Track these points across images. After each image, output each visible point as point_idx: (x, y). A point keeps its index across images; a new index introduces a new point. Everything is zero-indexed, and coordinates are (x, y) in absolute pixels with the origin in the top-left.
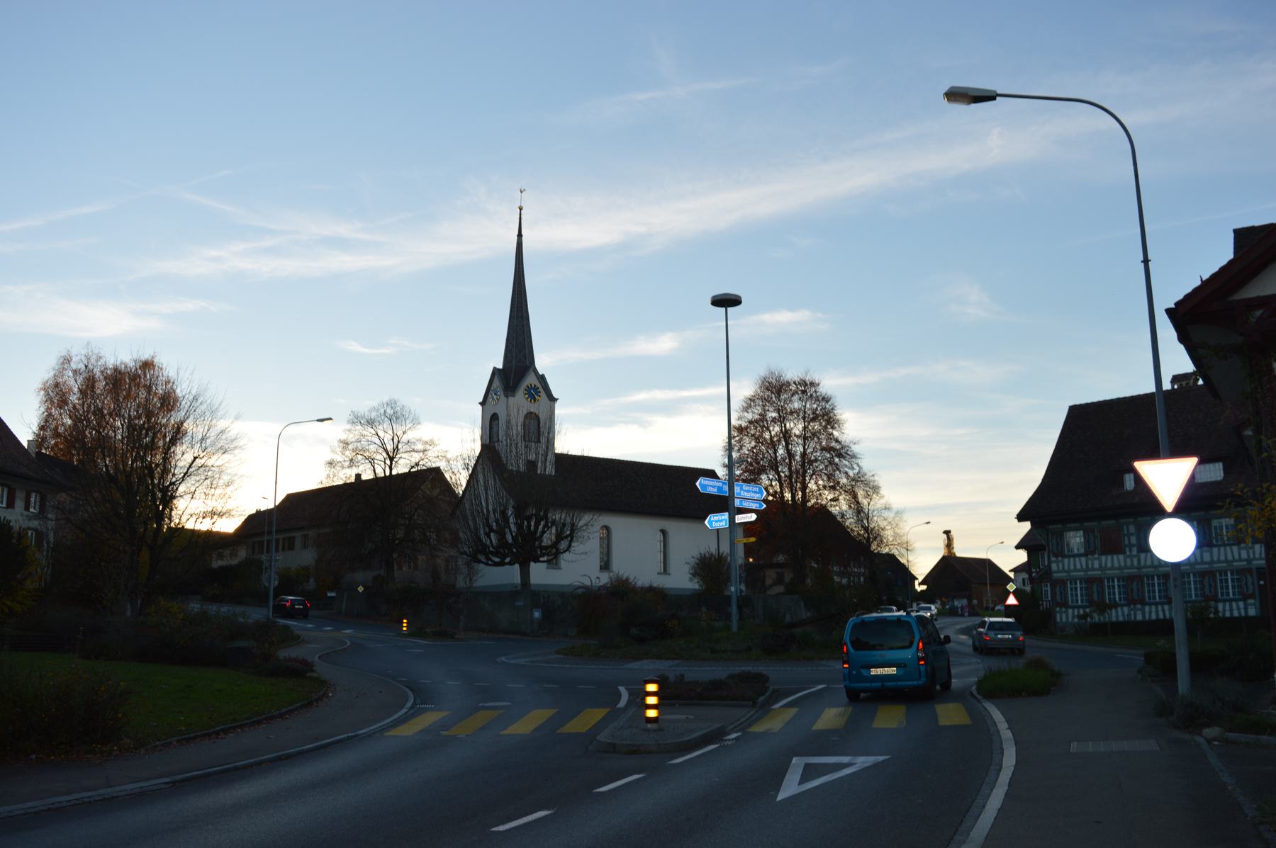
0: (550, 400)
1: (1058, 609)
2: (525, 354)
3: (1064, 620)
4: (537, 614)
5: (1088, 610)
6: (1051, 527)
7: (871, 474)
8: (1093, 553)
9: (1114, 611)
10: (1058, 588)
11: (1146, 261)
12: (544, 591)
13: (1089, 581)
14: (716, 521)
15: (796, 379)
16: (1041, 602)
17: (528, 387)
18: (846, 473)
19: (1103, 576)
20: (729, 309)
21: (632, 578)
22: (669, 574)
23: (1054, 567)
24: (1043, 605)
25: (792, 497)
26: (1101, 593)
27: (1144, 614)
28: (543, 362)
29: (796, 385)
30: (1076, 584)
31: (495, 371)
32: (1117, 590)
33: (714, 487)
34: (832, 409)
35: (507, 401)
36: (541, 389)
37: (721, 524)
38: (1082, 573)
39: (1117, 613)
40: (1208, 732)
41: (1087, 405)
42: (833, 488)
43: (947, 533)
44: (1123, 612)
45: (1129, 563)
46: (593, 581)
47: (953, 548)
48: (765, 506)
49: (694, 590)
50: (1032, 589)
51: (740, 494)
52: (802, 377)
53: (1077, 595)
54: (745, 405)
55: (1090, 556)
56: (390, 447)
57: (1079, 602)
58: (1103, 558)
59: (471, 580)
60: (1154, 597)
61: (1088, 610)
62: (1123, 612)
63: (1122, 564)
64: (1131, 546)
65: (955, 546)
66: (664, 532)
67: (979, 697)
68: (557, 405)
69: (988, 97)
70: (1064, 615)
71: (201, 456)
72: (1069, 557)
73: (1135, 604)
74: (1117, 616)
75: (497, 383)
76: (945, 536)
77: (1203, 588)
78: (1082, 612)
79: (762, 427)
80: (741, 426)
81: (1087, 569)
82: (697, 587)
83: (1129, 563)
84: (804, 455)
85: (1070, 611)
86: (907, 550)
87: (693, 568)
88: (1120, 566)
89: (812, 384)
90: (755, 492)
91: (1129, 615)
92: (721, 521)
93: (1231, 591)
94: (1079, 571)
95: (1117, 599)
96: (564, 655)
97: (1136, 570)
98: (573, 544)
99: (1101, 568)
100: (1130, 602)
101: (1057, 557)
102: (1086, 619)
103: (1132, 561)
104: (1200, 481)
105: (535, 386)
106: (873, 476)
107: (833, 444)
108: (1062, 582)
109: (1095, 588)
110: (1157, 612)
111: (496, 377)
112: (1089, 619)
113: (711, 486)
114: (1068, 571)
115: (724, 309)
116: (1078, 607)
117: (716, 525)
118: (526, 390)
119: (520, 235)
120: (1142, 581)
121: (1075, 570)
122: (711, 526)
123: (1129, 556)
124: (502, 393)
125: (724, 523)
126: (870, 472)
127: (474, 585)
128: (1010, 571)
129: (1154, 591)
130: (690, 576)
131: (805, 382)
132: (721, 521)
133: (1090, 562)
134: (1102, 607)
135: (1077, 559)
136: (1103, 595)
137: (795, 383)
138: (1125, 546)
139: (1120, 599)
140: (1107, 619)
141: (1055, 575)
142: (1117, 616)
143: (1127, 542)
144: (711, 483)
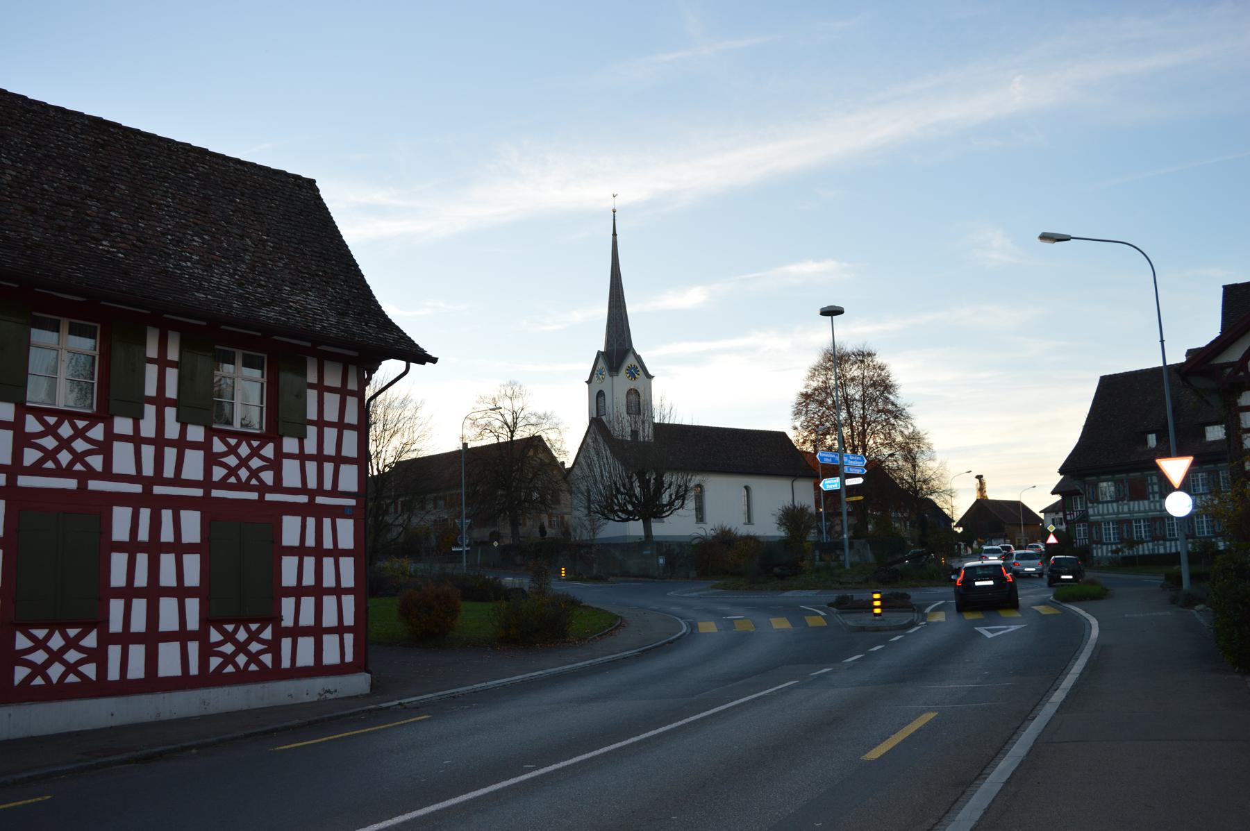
0: (647, 378)
1: (1094, 546)
3: (1100, 554)
4: (661, 561)
5: (1119, 546)
6: (1087, 479)
7: (924, 433)
8: (1123, 500)
9: (1141, 546)
10: (1094, 529)
11: (1162, 341)
12: (666, 542)
13: (1120, 523)
14: (830, 484)
15: (855, 350)
16: (1075, 541)
18: (902, 432)
19: (1131, 518)
20: (834, 317)
21: (733, 529)
22: (753, 524)
23: (1091, 511)
24: (1076, 542)
26: (1130, 532)
27: (1165, 548)
28: (640, 343)
29: (855, 355)
30: (1109, 525)
31: (599, 354)
32: (1143, 529)
33: (829, 458)
34: (888, 376)
35: (612, 380)
36: (639, 369)
37: (834, 486)
38: (1114, 516)
39: (1143, 548)
40: (1198, 607)
41: (1115, 375)
42: (890, 445)
43: (979, 477)
44: (1148, 547)
45: (1152, 508)
46: (708, 532)
47: (985, 492)
48: (866, 471)
49: (781, 537)
50: (1067, 528)
51: (847, 462)
52: (859, 348)
53: (1110, 534)
54: (810, 374)
55: (1120, 502)
56: (509, 420)
57: (1112, 539)
58: (1131, 503)
59: (594, 533)
60: (1174, 535)
61: (1119, 546)
62: (1148, 547)
63: (1147, 508)
64: (1154, 493)
65: (987, 490)
66: (747, 488)
67: (1058, 602)
68: (654, 382)
69: (1066, 238)
70: (1099, 551)
72: (1103, 503)
73: (1158, 541)
74: (1143, 550)
75: (601, 364)
76: (977, 481)
77: (1213, 527)
78: (1114, 547)
79: (827, 393)
80: (807, 392)
81: (1118, 513)
82: (783, 534)
83: (1152, 508)
84: (864, 417)
85: (1105, 547)
86: (952, 497)
87: (780, 519)
88: (1145, 510)
89: (870, 355)
90: (858, 461)
91: (1153, 549)
92: (834, 484)
93: (1112, 536)
94: (1111, 514)
95: (1143, 537)
96: (723, 589)
97: (1158, 513)
98: (686, 502)
99: (1130, 512)
100: (1154, 538)
101: (1093, 503)
102: (1118, 553)
103: (1155, 506)
104: (1210, 440)
105: (634, 366)
106: (926, 434)
107: (890, 407)
108: (1098, 524)
109: (1125, 528)
110: (1176, 546)
111: (600, 359)
112: (1120, 554)
113: (827, 458)
114: (1103, 515)
115: (830, 317)
116: (1112, 544)
117: (829, 488)
119: (615, 234)
120: (1164, 521)
121: (1108, 514)
122: (825, 487)
123: (1152, 502)
124: (607, 373)
125: (836, 485)
126: (923, 431)
127: (596, 538)
128: (1041, 512)
129: (1203, 527)
130: (778, 525)
131: (863, 352)
132: (834, 484)
133: (1120, 507)
134: (1132, 543)
135: (1110, 505)
136: (1194, 529)
137: (853, 354)
138: (1150, 493)
139: (1146, 536)
140: (1135, 553)
141: (1092, 518)
142: (1143, 550)
143: (1150, 491)
144: (827, 455)
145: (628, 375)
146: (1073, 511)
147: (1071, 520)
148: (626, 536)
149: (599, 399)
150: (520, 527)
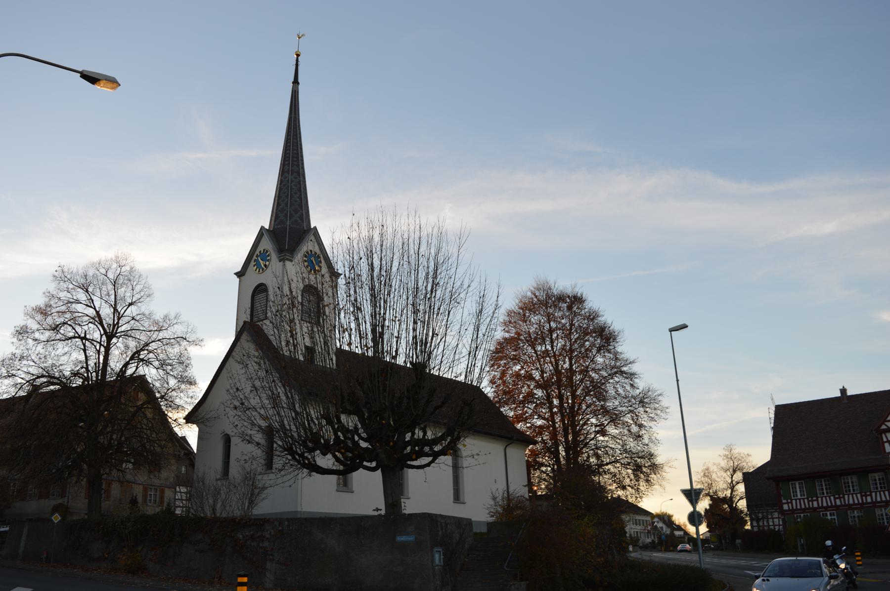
2: (302, 214)
17: (307, 252)
25: (423, 436)
31: (262, 232)
71: (651, 415)
118: (306, 256)
119: (296, 82)
137: (569, 296)
145: (306, 264)
146: (792, 500)
147: (789, 510)
148: (297, 511)
149: (256, 298)
150: (55, 376)
